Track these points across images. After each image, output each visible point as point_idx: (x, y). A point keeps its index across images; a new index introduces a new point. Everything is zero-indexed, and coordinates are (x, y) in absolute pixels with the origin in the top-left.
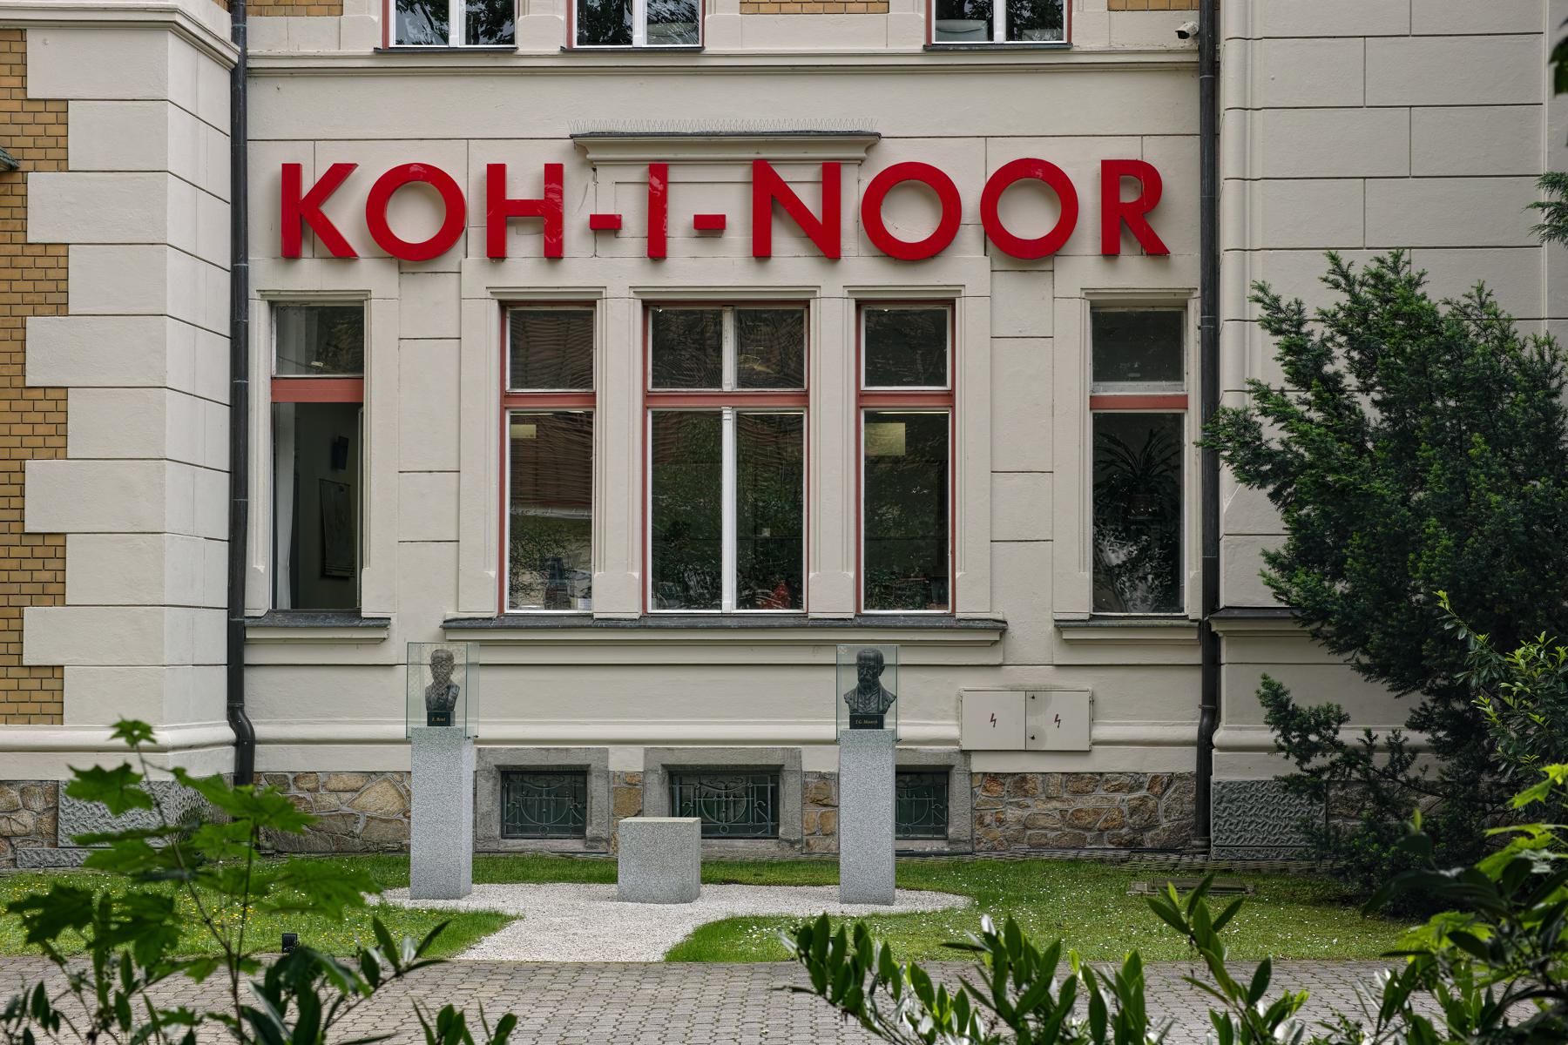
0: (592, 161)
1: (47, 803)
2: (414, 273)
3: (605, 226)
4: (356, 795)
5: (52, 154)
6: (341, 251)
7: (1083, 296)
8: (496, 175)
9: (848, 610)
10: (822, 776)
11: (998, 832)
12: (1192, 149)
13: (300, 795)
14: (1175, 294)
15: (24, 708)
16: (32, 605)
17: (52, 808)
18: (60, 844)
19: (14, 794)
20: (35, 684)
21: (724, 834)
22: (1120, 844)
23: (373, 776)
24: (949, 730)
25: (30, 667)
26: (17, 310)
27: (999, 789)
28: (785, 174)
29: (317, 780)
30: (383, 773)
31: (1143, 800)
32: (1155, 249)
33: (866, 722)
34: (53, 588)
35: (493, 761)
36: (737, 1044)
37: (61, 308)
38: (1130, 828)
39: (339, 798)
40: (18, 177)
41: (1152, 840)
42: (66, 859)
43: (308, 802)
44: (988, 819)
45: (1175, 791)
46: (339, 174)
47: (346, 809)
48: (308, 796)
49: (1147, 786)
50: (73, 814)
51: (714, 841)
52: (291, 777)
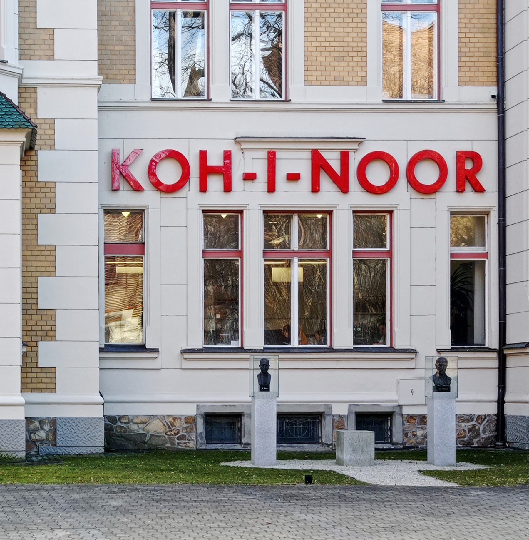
0: (242, 149)
1: (51, 427)
2: (166, 197)
3: (250, 177)
4: (145, 425)
5: (48, 142)
6: (137, 188)
7: (448, 209)
8: (203, 155)
9: (351, 346)
10: (340, 416)
11: (413, 440)
12: (494, 147)
13: (122, 425)
14: (486, 209)
15: (39, 386)
16: (41, 340)
17: (53, 429)
18: (57, 445)
19: (37, 423)
20: (43, 375)
21: (298, 442)
22: (464, 444)
23: (152, 417)
24: (393, 396)
25: (41, 368)
26: (34, 211)
27: (414, 421)
28: (326, 155)
29: (128, 418)
30: (156, 416)
31: (474, 426)
32: (479, 189)
33: (443, 389)
34: (51, 333)
35: (204, 411)
36: (32, 539)
37: (52, 210)
38: (468, 437)
39: (138, 427)
40: (33, 153)
41: (477, 442)
42: (60, 451)
43: (125, 428)
44: (409, 435)
45: (487, 422)
46: (137, 153)
47: (141, 432)
48: (125, 426)
49: (475, 420)
50: (63, 432)
51: (295, 445)
52: (117, 418)
